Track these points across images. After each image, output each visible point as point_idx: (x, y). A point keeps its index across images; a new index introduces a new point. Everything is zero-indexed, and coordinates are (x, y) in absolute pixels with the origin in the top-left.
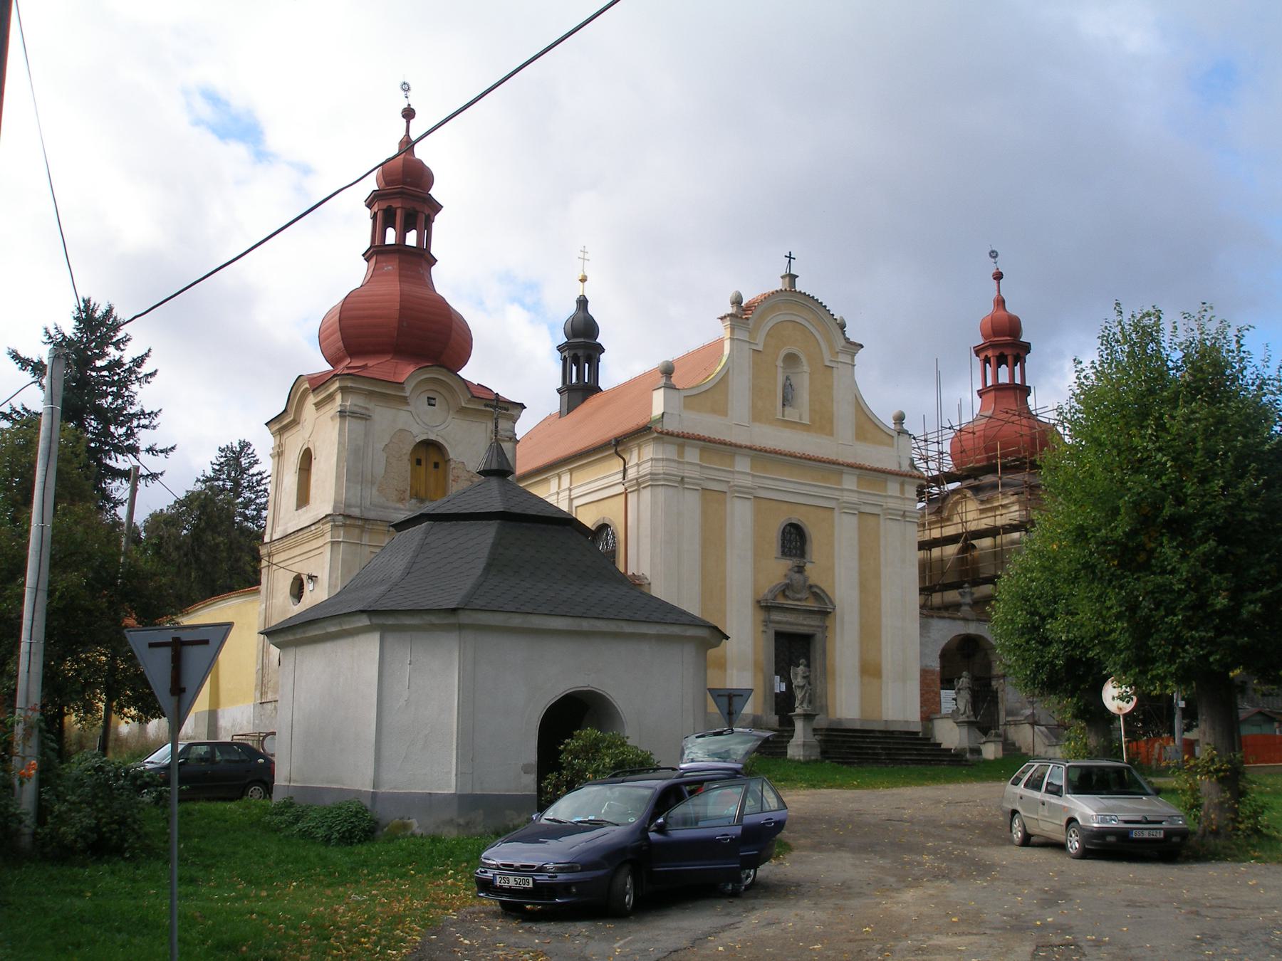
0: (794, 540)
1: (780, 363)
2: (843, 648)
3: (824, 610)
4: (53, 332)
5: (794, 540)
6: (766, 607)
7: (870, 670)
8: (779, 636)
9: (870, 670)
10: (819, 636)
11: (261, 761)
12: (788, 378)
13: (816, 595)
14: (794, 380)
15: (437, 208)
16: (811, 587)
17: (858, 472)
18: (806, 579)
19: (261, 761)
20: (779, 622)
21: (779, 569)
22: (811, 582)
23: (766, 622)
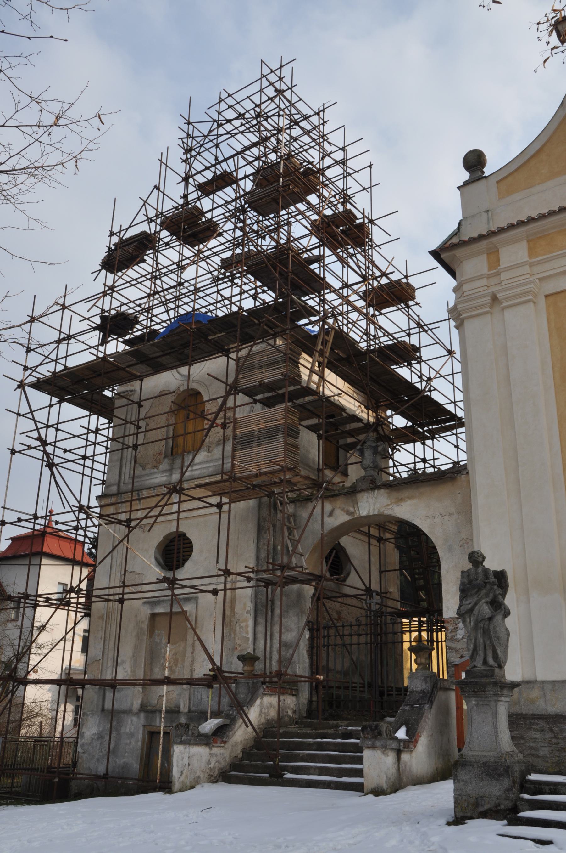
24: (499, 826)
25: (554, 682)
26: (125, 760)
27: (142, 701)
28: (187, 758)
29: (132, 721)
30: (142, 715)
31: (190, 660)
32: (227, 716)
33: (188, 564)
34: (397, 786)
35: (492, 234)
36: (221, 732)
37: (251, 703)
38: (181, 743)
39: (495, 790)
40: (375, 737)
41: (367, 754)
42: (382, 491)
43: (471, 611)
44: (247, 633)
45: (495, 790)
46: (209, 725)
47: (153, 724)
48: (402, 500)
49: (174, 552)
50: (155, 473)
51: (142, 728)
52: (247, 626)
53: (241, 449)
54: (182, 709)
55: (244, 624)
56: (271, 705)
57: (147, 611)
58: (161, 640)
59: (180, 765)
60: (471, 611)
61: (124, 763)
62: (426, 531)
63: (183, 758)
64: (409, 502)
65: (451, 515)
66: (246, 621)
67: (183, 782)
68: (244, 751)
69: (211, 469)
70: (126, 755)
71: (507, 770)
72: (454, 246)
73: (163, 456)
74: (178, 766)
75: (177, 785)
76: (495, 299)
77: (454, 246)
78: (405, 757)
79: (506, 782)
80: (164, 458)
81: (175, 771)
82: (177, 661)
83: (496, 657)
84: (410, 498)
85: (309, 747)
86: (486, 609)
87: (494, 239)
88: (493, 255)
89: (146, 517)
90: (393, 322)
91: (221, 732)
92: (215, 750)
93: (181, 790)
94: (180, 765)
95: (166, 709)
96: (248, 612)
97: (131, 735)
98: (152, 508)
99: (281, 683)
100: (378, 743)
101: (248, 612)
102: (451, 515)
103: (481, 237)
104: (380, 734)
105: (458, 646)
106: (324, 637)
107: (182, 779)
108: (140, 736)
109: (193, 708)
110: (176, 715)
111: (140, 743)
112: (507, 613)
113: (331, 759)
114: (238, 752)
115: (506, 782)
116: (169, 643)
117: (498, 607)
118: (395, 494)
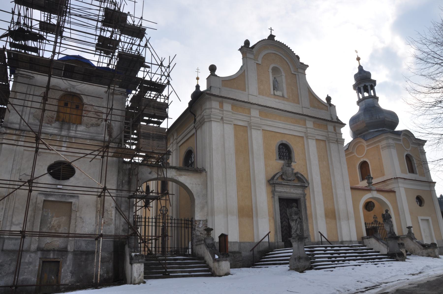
0: (285, 152)
1: (270, 70)
2: (316, 204)
3: (302, 181)
4: (422, 56)
5: (285, 152)
6: (272, 182)
7: (331, 215)
8: (281, 200)
9: (331, 215)
10: (302, 199)
11: (135, 131)
12: (275, 78)
13: (298, 178)
14: (278, 79)
15: (304, 67)
16: (296, 174)
17: (313, 120)
18: (293, 170)
19: (135, 131)
20: (280, 192)
21: (277, 165)
22: (295, 171)
23: (273, 192)
25: (234, 242)
26: (24, 277)
27: (38, 246)
29: (30, 256)
30: (39, 253)
31: (74, 226)
33: (72, 179)
40: (227, 257)
42: (174, 170)
44: (112, 217)
47: (48, 257)
48: (181, 175)
49: (62, 171)
50: (49, 127)
51: (39, 259)
52: (111, 214)
53: (143, 139)
54: (69, 248)
55: (110, 213)
57: (42, 198)
58: (48, 214)
59: (138, 272)
61: (24, 278)
62: (190, 188)
63: (140, 269)
64: (184, 177)
65: (199, 184)
66: (111, 211)
67: (141, 279)
69: (88, 136)
70: (26, 274)
73: (54, 119)
74: (137, 272)
76: (222, 119)
80: (56, 121)
82: (60, 225)
84: (184, 175)
87: (224, 99)
88: (221, 104)
89: (90, 154)
94: (138, 272)
96: (112, 207)
97: (30, 263)
98: (95, 151)
100: (228, 259)
101: (112, 207)
102: (199, 184)
104: (229, 256)
106: (139, 222)
107: (140, 278)
108: (38, 264)
110: (66, 253)
111: (37, 268)
116: (103, 218)
118: (178, 172)
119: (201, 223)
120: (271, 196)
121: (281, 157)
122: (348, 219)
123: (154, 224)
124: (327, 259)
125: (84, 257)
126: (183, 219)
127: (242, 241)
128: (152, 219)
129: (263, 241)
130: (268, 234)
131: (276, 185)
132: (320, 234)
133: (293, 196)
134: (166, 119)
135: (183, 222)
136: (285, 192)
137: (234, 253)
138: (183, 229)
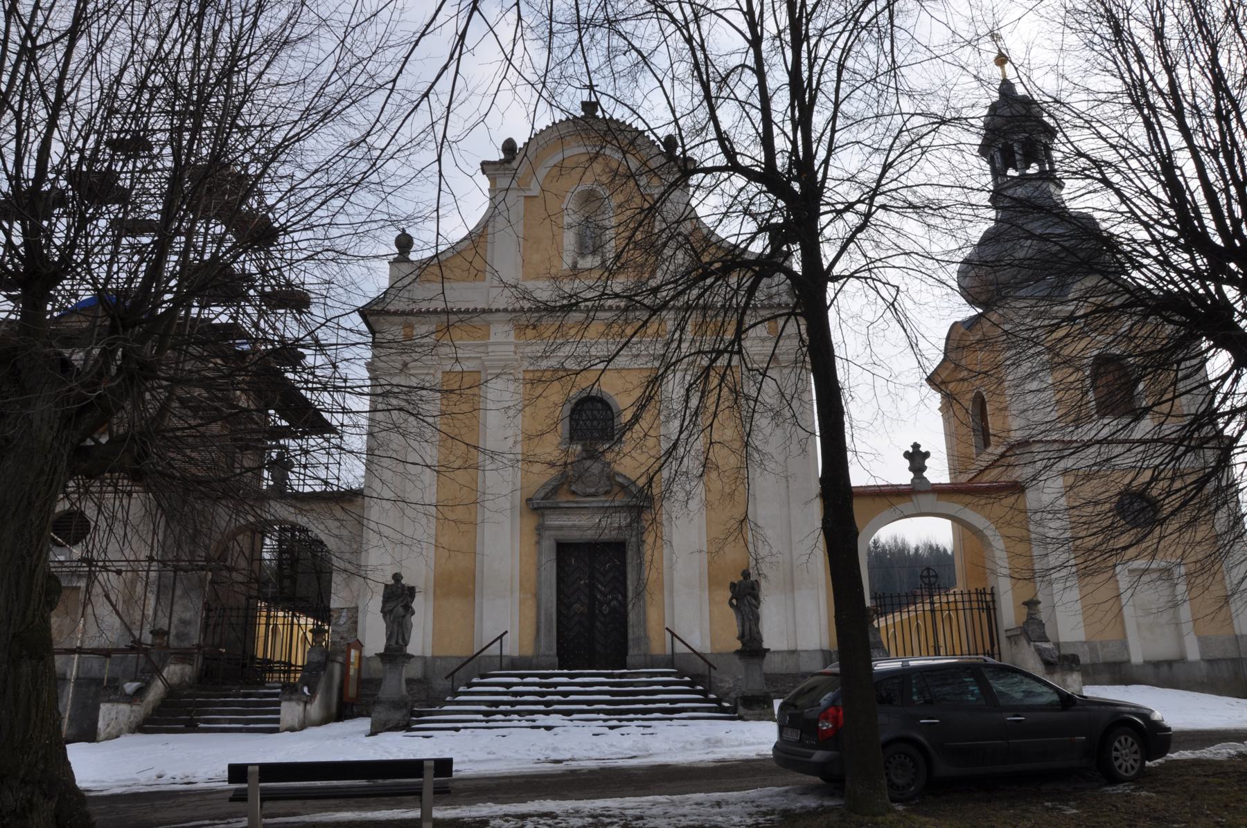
0: (592, 421)
8: (564, 550)
20: (561, 528)
23: (540, 529)
24: (402, 733)
28: (109, 714)
32: (143, 681)
34: (302, 727)
35: (411, 313)
36: (140, 693)
37: (163, 668)
38: (109, 701)
39: (397, 716)
40: (292, 693)
41: (284, 704)
43: (391, 611)
45: (397, 716)
46: (130, 687)
56: (175, 673)
60: (391, 611)
68: (153, 709)
71: (406, 704)
72: (379, 313)
75: (102, 735)
77: (379, 313)
78: (308, 707)
79: (404, 711)
81: (101, 725)
83: (404, 639)
85: (216, 704)
86: (401, 610)
90: (290, 327)
91: (140, 693)
92: (135, 708)
93: (108, 738)
95: (77, 678)
99: (183, 656)
100: (294, 697)
103: (403, 313)
105: (340, 629)
109: (81, 675)
112: (413, 613)
113: (237, 713)
114: (150, 710)
115: (404, 711)
117: (409, 610)
119: (344, 614)
120: (534, 539)
121: (575, 434)
122: (793, 590)
123: (967, 605)
124: (608, 697)
125: (93, 689)
126: (973, 591)
127: (442, 654)
128: (969, 593)
129: (484, 653)
130: (501, 637)
131: (547, 512)
132: (668, 635)
133: (608, 536)
134: (934, 356)
135: (974, 597)
136: (574, 526)
137: (1086, 666)
138: (976, 612)
